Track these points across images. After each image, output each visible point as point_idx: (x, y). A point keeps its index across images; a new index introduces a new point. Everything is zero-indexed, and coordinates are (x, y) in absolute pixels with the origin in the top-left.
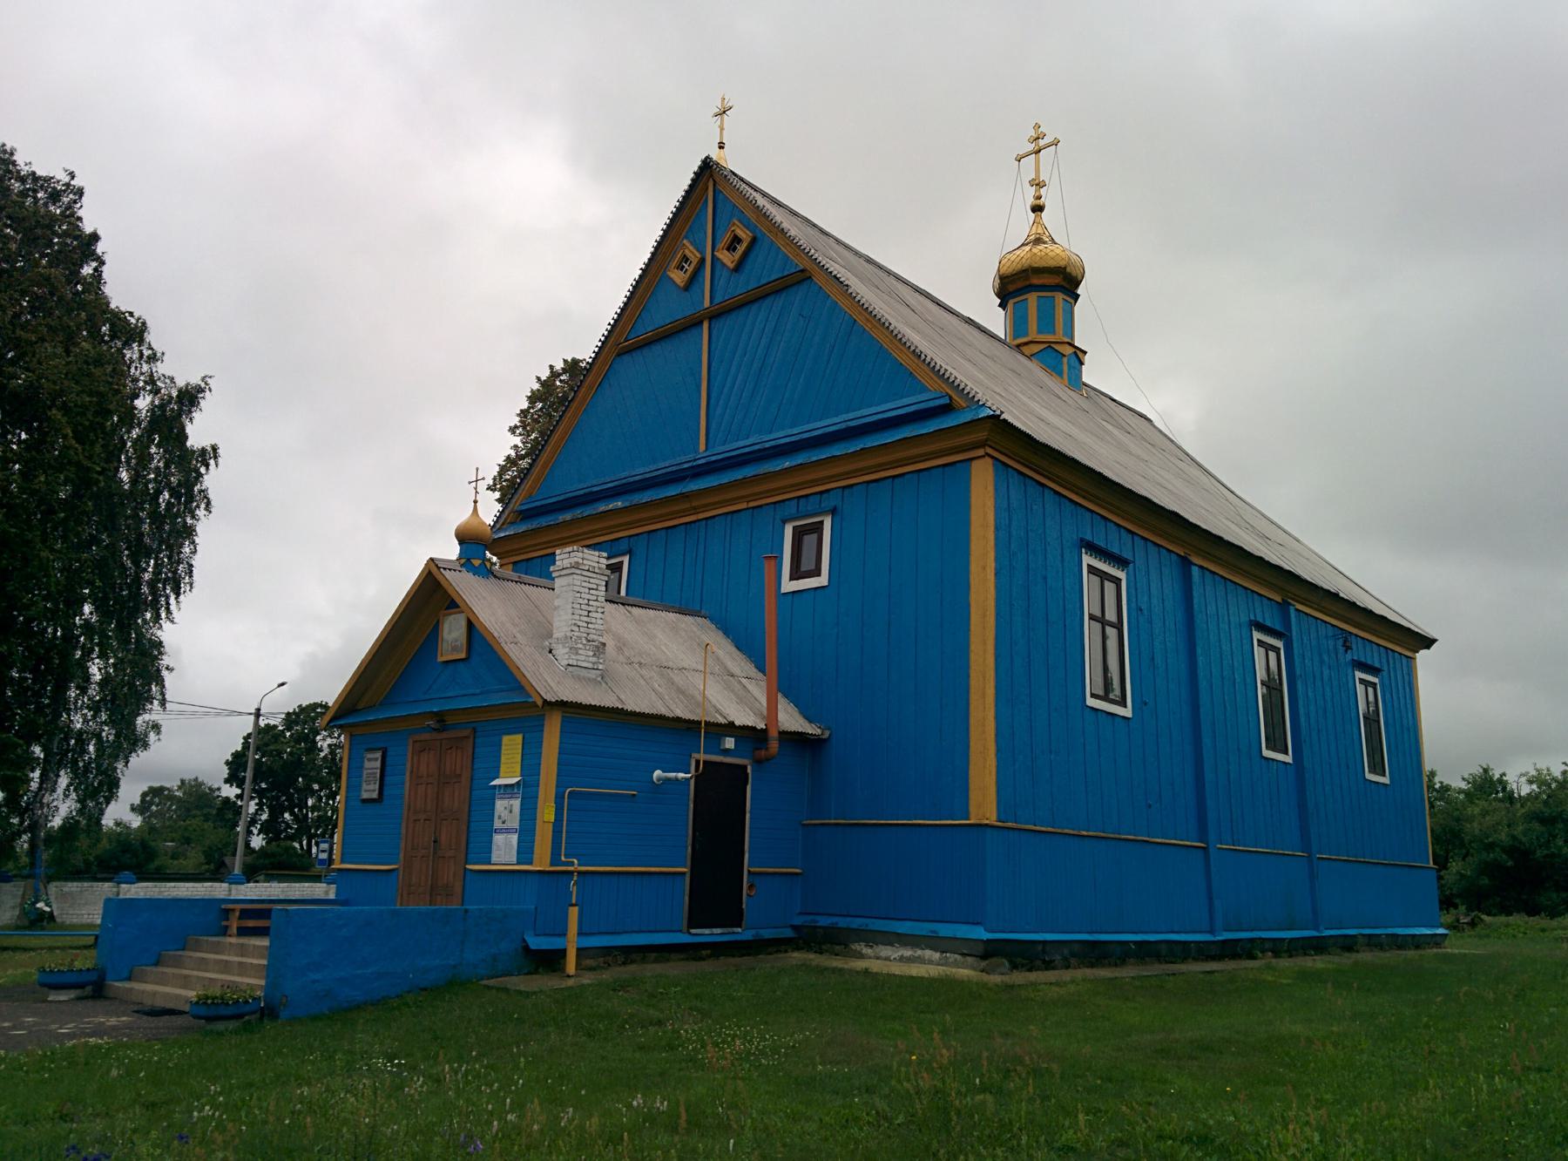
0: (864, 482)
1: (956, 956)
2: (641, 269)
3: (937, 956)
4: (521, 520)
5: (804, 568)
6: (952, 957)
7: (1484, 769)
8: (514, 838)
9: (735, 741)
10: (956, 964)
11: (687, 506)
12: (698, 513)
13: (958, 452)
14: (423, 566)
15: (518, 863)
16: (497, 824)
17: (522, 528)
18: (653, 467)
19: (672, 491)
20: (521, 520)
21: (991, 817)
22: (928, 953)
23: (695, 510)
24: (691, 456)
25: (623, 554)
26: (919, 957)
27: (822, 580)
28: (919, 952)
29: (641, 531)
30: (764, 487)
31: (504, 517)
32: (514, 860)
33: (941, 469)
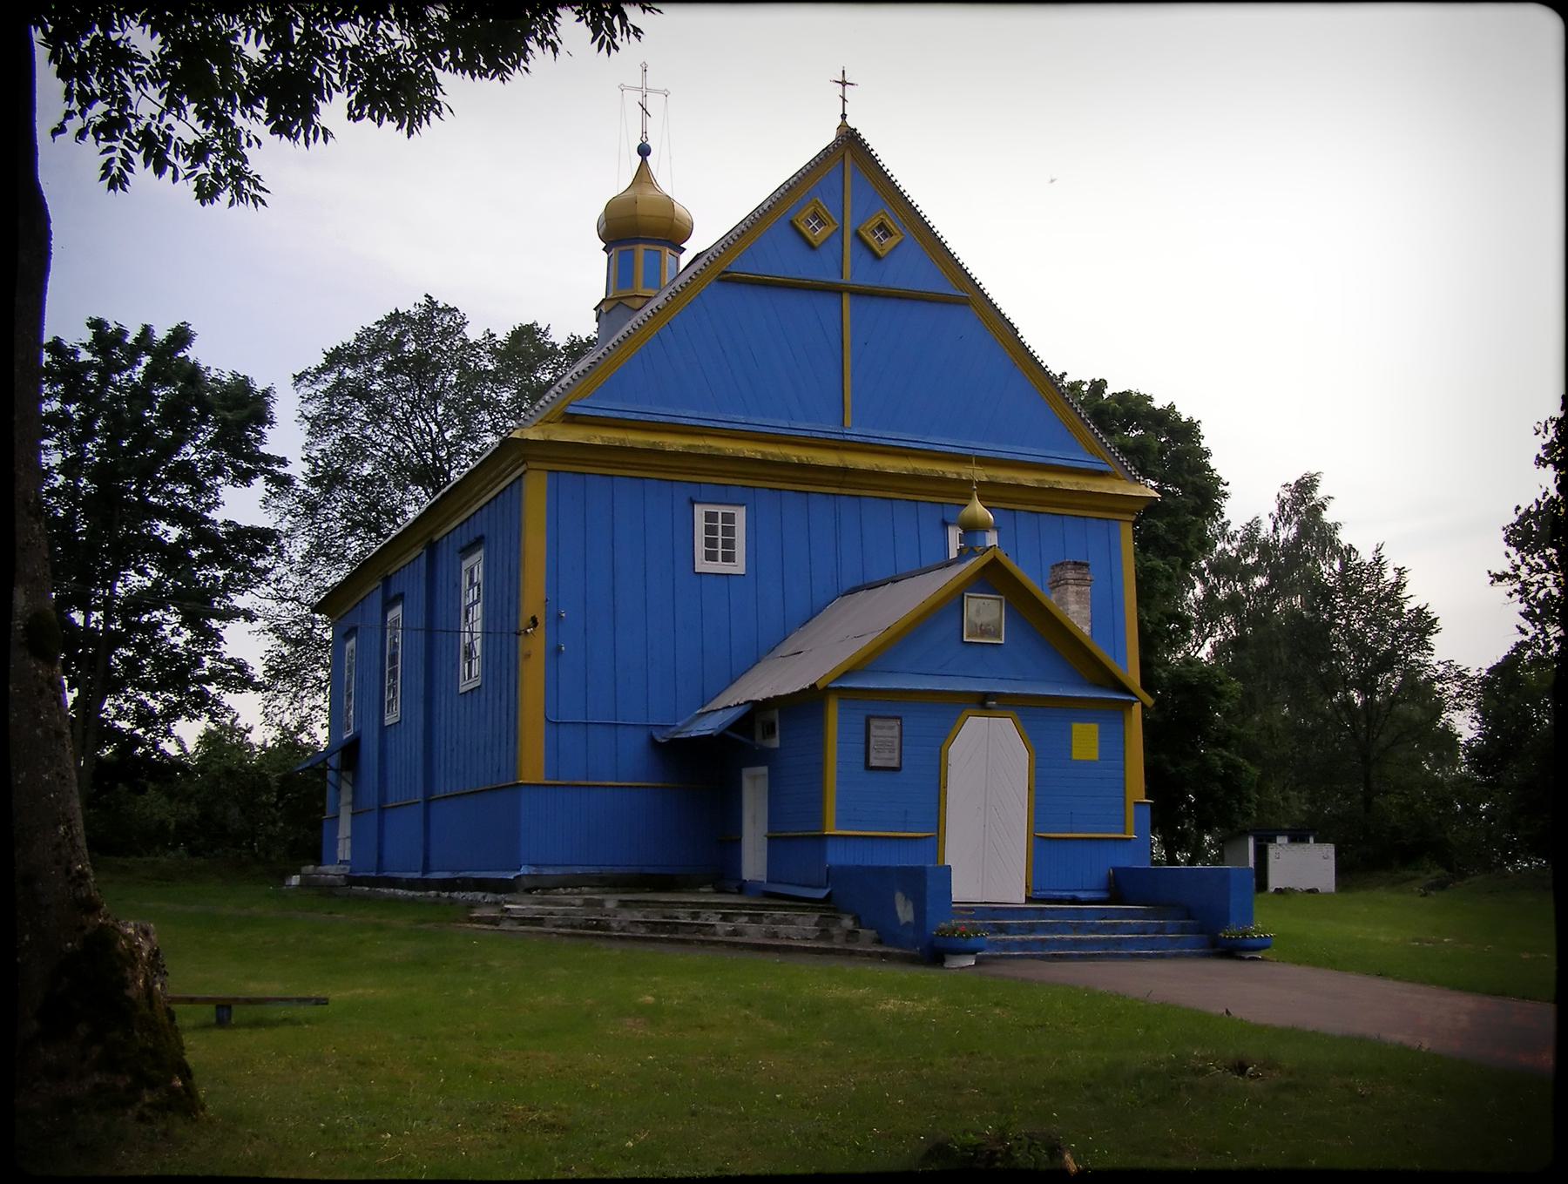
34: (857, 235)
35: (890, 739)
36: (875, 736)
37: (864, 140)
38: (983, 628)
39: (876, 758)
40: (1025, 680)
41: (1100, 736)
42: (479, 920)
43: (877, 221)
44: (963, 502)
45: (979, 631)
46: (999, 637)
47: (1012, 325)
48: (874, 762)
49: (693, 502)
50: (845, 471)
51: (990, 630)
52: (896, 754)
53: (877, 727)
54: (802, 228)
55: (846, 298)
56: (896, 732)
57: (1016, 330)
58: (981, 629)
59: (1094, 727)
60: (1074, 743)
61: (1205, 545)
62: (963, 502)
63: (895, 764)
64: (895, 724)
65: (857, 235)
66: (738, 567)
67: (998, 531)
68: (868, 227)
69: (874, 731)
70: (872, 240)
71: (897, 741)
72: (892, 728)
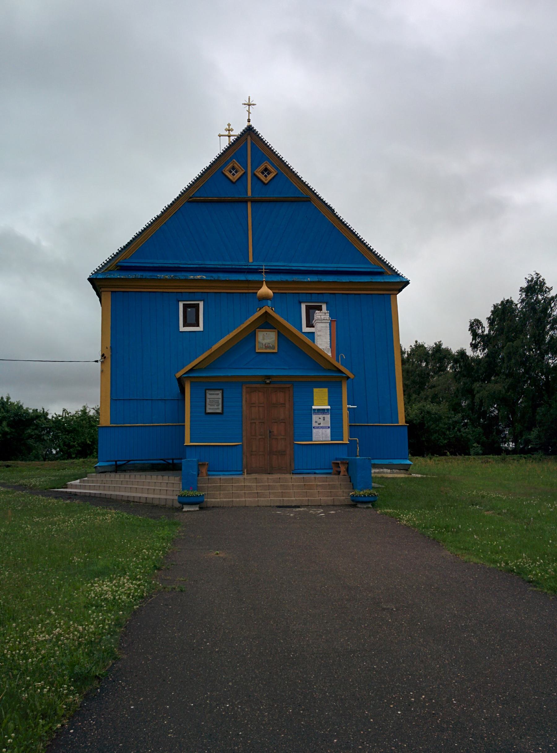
0: (214, 292)
1: (397, 470)
2: (210, 162)
3: (389, 471)
4: (117, 270)
5: (188, 322)
6: (395, 471)
7: (96, 411)
8: (329, 431)
9: (329, 392)
10: (397, 473)
11: (247, 285)
12: (249, 289)
13: (383, 291)
14: (403, 290)
15: (331, 440)
16: (314, 424)
17: (117, 275)
18: (220, 263)
19: (242, 277)
20: (117, 270)
21: (108, 424)
22: (385, 470)
23: (248, 288)
24: (243, 263)
25: (201, 300)
26: (382, 472)
27: (201, 328)
28: (382, 470)
29: (118, 290)
30: (372, 287)
31: (109, 265)
32: (330, 439)
33: (317, 295)
34: (254, 175)
35: (217, 400)
36: (210, 399)
37: (258, 132)
38: (266, 345)
39: (210, 409)
40: (289, 369)
41: (329, 394)
42: (185, 512)
43: (230, 166)
44: (259, 286)
45: (264, 347)
46: (274, 349)
47: (331, 208)
48: (208, 411)
49: (179, 301)
50: (248, 281)
51: (270, 346)
52: (220, 406)
53: (210, 394)
54: (227, 174)
55: (249, 204)
56: (220, 396)
57: (333, 210)
58: (265, 346)
59: (326, 390)
60: (315, 398)
61: (514, 310)
62: (259, 286)
63: (220, 411)
64: (220, 392)
65: (254, 175)
66: (201, 328)
67: (326, 304)
68: (259, 170)
69: (208, 396)
70: (262, 177)
71: (220, 401)
72: (218, 394)
